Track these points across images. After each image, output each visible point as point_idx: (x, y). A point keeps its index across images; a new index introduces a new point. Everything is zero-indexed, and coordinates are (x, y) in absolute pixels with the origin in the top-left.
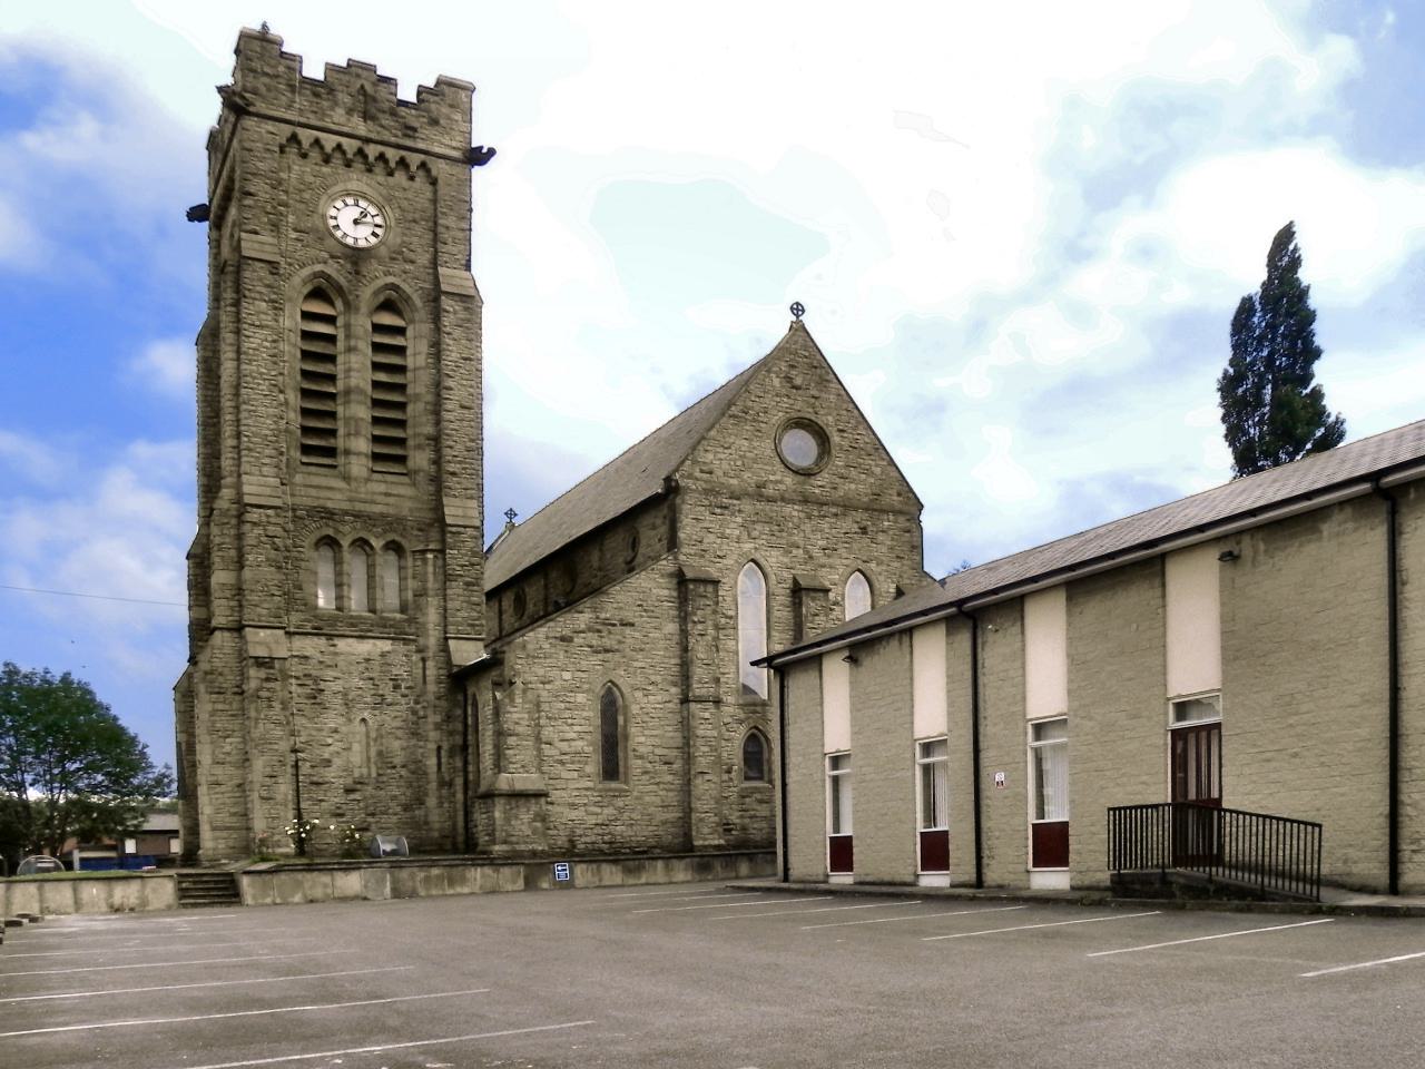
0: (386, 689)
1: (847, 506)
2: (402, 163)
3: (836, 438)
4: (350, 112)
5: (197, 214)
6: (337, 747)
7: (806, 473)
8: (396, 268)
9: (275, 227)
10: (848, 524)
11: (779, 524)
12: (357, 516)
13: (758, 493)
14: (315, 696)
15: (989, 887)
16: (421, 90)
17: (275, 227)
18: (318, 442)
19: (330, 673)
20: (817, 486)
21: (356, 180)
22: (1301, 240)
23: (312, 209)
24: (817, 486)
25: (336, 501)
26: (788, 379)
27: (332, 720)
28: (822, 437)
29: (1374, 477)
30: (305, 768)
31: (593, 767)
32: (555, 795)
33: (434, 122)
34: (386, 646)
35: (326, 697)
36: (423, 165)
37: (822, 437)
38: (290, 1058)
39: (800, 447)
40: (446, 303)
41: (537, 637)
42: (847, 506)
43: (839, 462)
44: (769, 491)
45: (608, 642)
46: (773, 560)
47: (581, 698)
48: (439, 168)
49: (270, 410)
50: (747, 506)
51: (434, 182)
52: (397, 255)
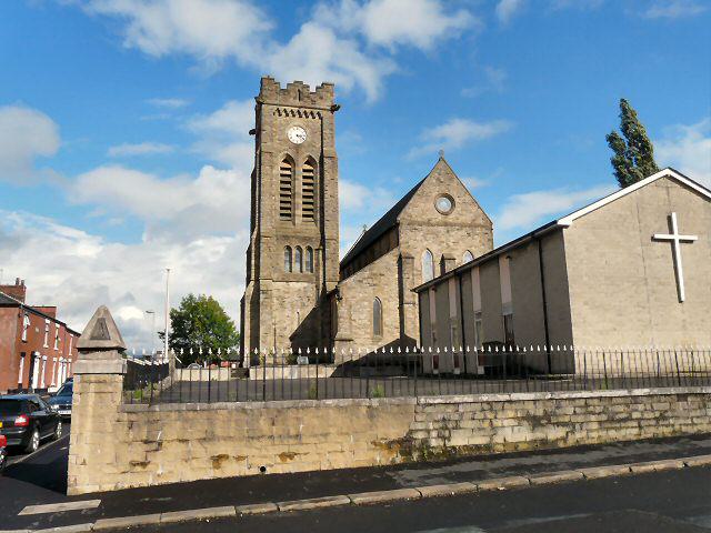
0: (305, 300)
1: (462, 226)
2: (312, 113)
3: (457, 200)
4: (295, 98)
5: (252, 132)
6: (288, 322)
7: (446, 214)
8: (311, 149)
9: (272, 140)
10: (464, 232)
11: (436, 235)
12: (297, 238)
13: (429, 223)
14: (282, 305)
15: (586, 382)
16: (317, 88)
17: (272, 140)
18: (287, 213)
19: (287, 296)
20: (451, 219)
21: (297, 120)
22: (631, 106)
23: (283, 132)
24: (451, 219)
25: (290, 233)
26: (438, 179)
27: (287, 313)
28: (451, 199)
29: (533, 233)
30: (278, 331)
31: (370, 330)
32: (356, 341)
33: (321, 98)
34: (306, 284)
35: (286, 304)
36: (318, 113)
37: (451, 199)
38: (520, 481)
39: (444, 205)
40: (326, 160)
41: (350, 281)
42: (462, 226)
43: (458, 209)
44: (433, 221)
45: (375, 282)
46: (434, 248)
47: (366, 303)
48: (323, 113)
49: (271, 202)
50: (424, 228)
51: (321, 118)
52: (311, 145)
